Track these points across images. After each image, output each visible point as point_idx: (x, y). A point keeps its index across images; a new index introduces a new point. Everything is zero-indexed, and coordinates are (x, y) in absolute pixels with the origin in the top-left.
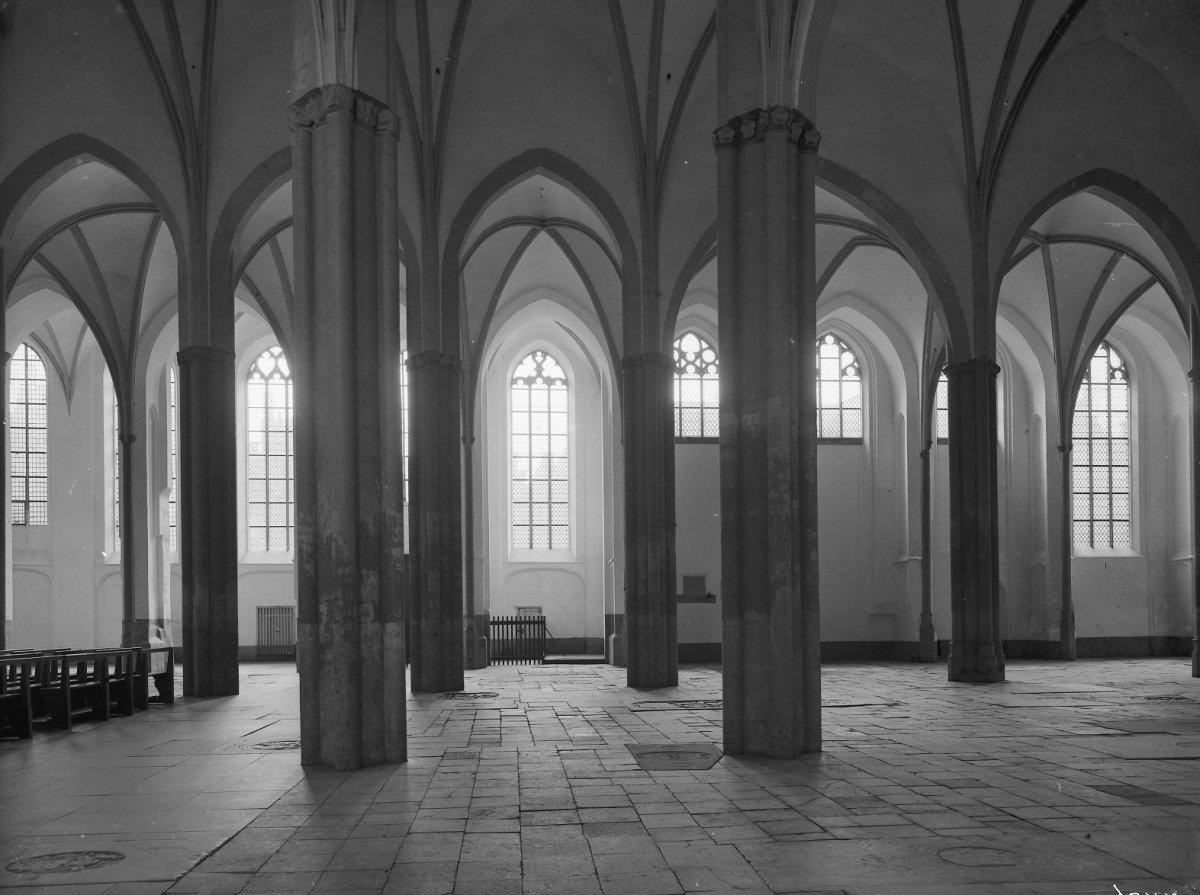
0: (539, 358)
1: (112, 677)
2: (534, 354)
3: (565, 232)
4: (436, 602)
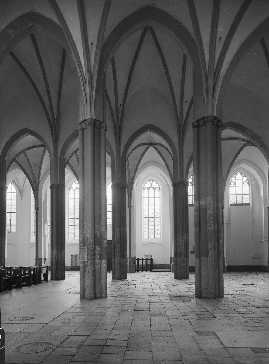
0: (151, 182)
1: (32, 274)
2: (150, 181)
3: (157, 146)
4: (119, 254)
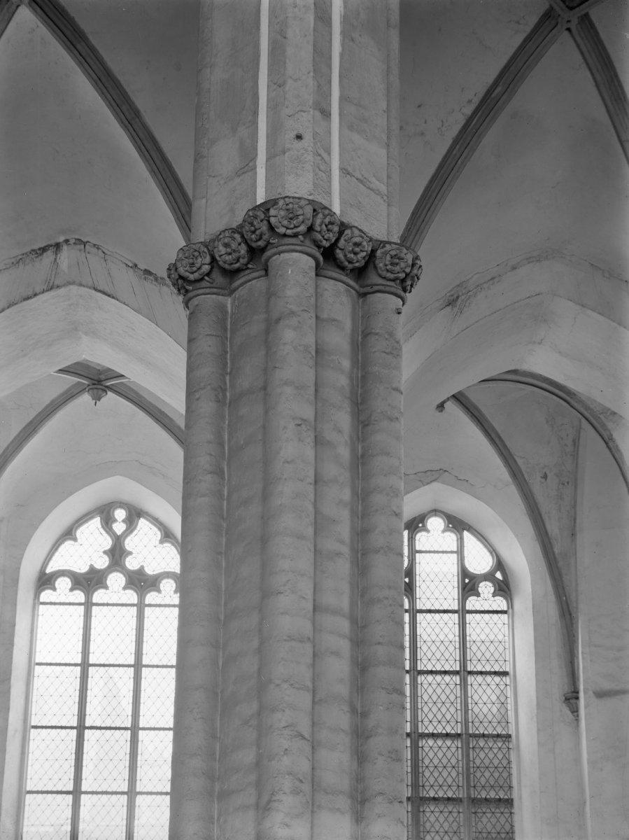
2: (105, 513)
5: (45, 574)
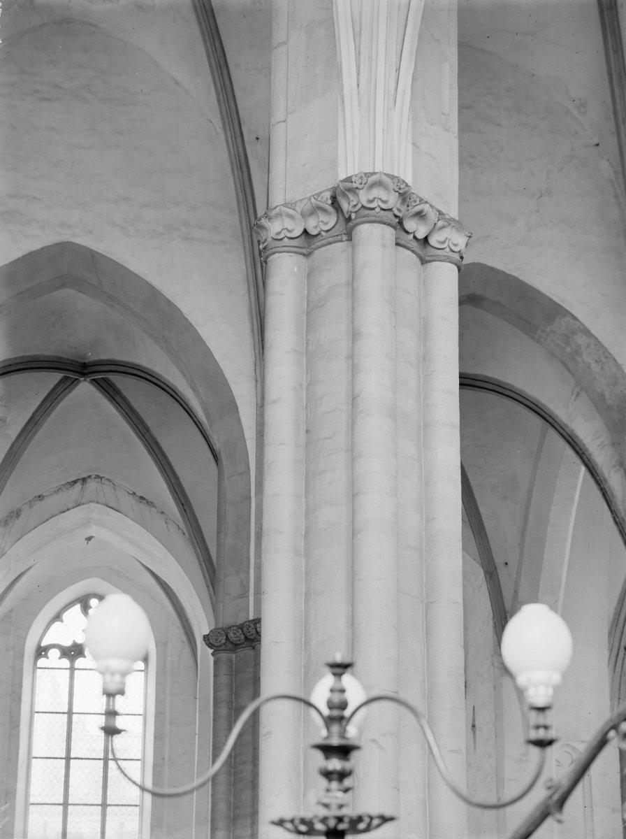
5: (41, 647)
